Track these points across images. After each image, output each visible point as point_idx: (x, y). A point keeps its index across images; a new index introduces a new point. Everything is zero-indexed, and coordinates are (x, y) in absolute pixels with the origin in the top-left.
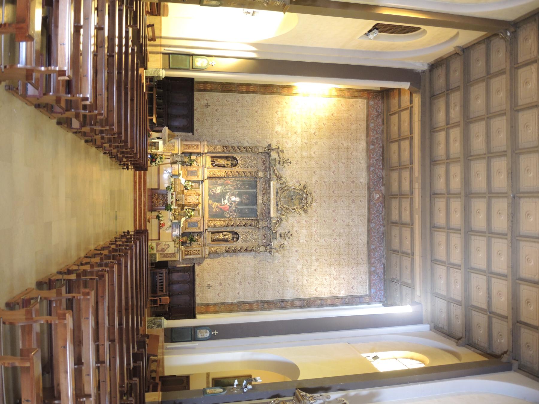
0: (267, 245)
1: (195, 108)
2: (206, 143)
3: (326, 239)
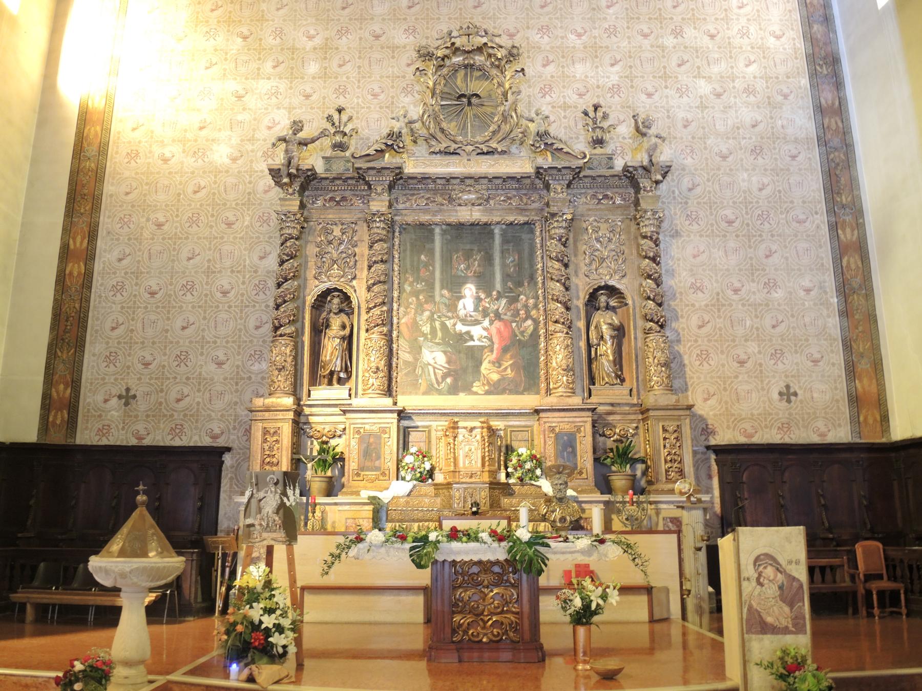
1: (133, 442)
2: (259, 402)
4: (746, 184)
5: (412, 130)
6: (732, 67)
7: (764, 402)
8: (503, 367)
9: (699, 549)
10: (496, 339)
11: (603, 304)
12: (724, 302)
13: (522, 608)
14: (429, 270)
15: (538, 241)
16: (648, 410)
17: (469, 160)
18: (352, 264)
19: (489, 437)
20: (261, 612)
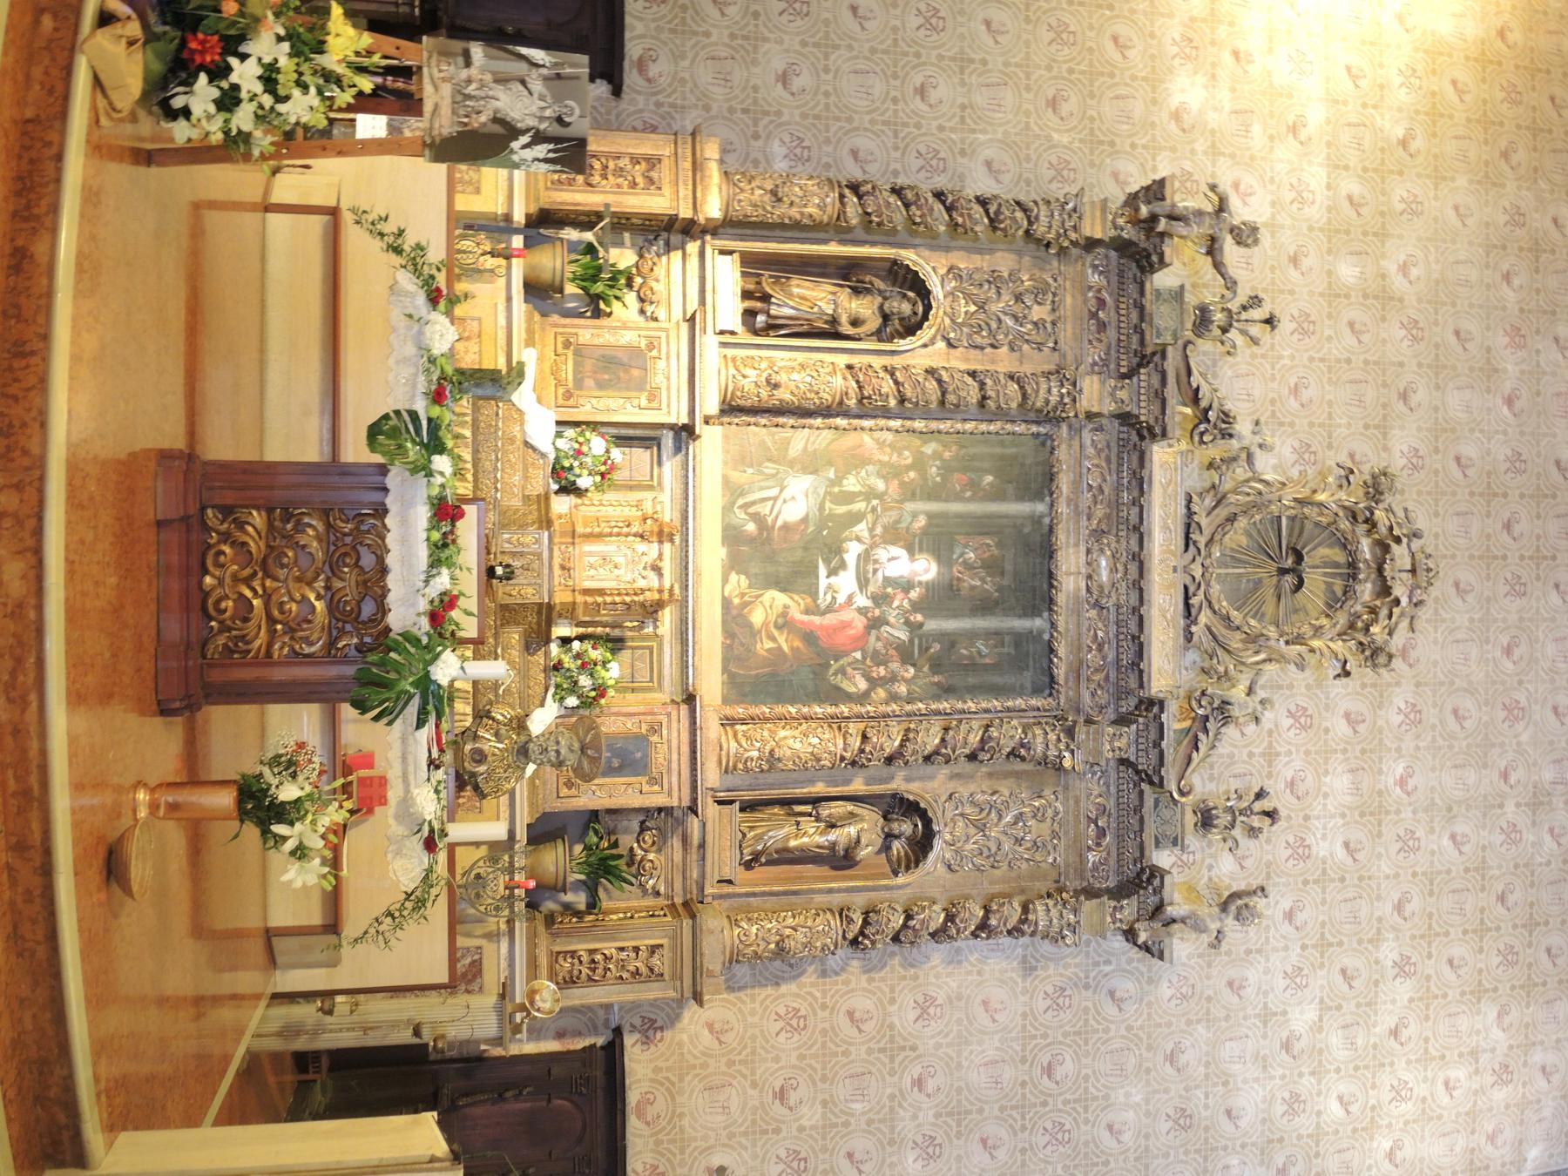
0: (1135, 892)
2: (711, 151)
3: (1460, 828)
4: (1122, 1099)
5: (1234, 459)
6: (1338, 1070)
7: (705, 1138)
8: (776, 633)
9: (417, 1033)
10: (830, 619)
11: (896, 827)
12: (898, 1060)
13: (279, 664)
14: (963, 491)
15: (1019, 702)
16: (693, 917)
17: (1175, 569)
18: (978, 340)
19: (642, 605)
20: (267, 60)
